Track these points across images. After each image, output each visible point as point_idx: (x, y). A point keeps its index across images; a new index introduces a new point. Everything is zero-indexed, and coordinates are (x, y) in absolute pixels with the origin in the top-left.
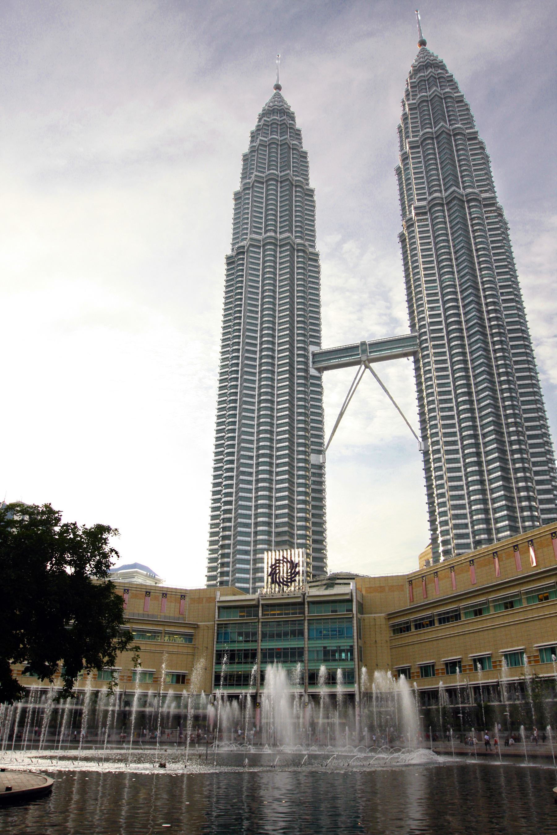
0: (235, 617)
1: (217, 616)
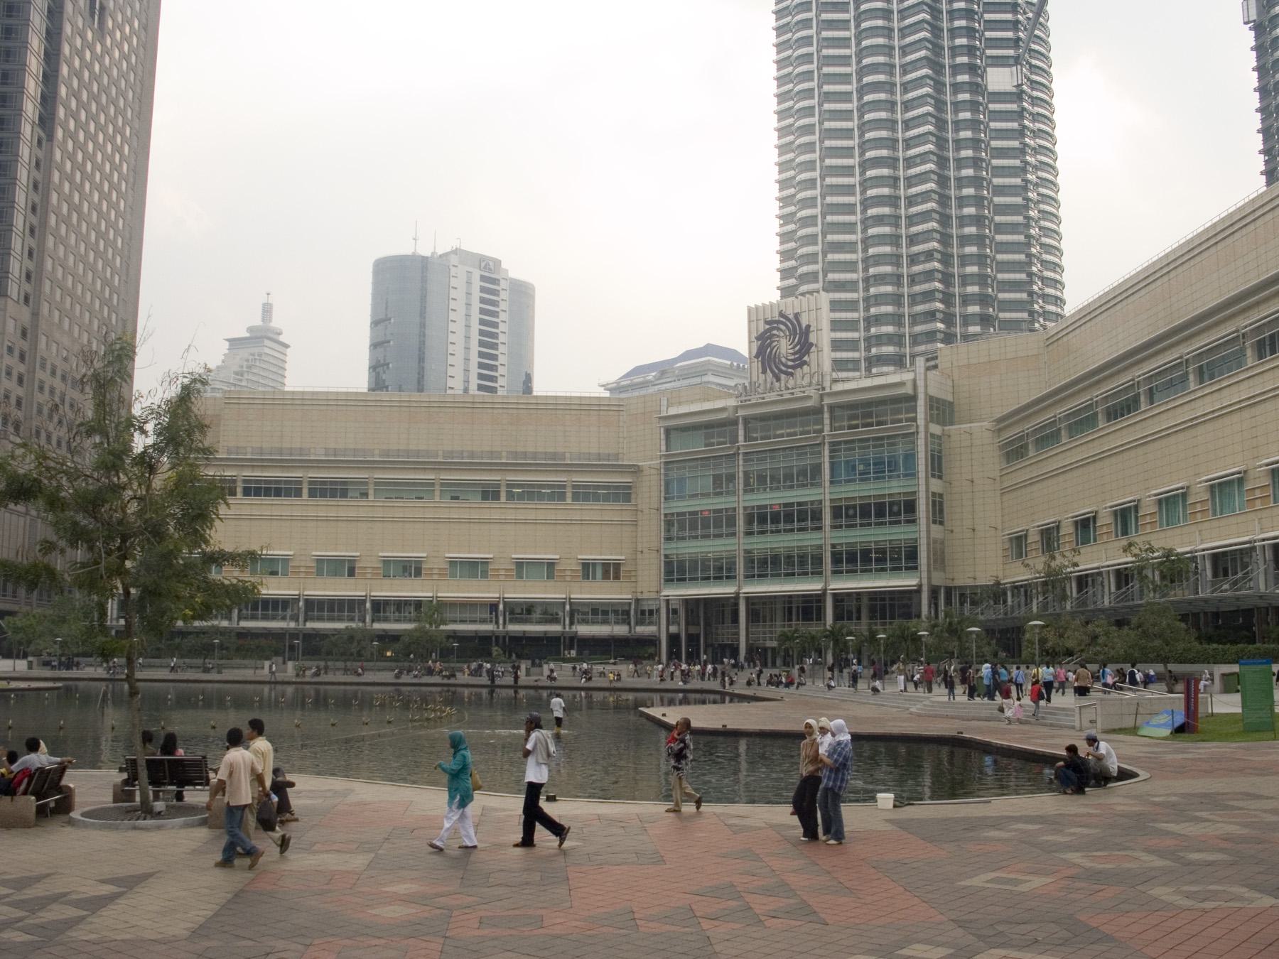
0: (696, 446)
1: (663, 448)
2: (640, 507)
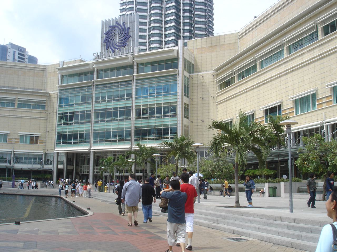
1: (60, 83)
2: (49, 112)
